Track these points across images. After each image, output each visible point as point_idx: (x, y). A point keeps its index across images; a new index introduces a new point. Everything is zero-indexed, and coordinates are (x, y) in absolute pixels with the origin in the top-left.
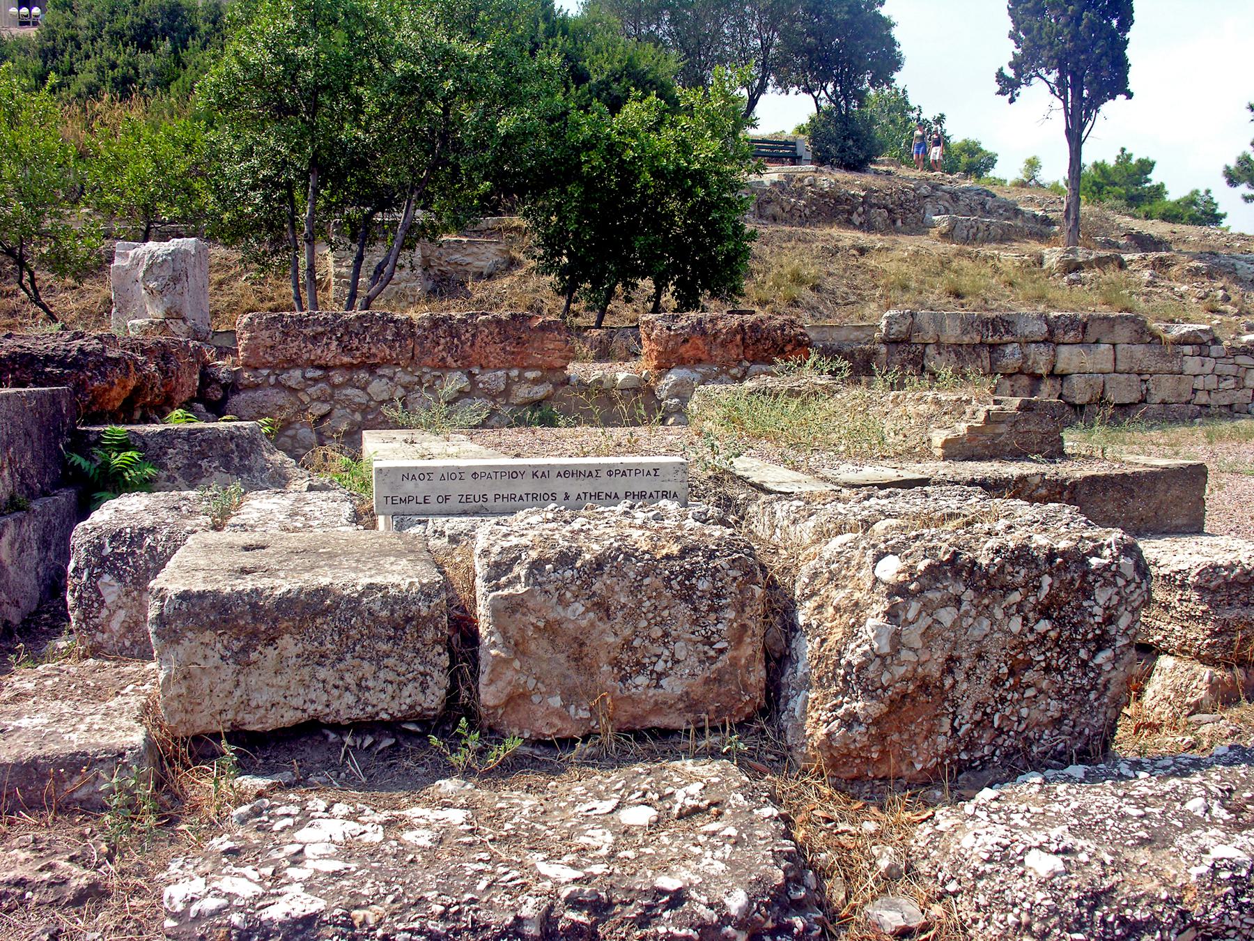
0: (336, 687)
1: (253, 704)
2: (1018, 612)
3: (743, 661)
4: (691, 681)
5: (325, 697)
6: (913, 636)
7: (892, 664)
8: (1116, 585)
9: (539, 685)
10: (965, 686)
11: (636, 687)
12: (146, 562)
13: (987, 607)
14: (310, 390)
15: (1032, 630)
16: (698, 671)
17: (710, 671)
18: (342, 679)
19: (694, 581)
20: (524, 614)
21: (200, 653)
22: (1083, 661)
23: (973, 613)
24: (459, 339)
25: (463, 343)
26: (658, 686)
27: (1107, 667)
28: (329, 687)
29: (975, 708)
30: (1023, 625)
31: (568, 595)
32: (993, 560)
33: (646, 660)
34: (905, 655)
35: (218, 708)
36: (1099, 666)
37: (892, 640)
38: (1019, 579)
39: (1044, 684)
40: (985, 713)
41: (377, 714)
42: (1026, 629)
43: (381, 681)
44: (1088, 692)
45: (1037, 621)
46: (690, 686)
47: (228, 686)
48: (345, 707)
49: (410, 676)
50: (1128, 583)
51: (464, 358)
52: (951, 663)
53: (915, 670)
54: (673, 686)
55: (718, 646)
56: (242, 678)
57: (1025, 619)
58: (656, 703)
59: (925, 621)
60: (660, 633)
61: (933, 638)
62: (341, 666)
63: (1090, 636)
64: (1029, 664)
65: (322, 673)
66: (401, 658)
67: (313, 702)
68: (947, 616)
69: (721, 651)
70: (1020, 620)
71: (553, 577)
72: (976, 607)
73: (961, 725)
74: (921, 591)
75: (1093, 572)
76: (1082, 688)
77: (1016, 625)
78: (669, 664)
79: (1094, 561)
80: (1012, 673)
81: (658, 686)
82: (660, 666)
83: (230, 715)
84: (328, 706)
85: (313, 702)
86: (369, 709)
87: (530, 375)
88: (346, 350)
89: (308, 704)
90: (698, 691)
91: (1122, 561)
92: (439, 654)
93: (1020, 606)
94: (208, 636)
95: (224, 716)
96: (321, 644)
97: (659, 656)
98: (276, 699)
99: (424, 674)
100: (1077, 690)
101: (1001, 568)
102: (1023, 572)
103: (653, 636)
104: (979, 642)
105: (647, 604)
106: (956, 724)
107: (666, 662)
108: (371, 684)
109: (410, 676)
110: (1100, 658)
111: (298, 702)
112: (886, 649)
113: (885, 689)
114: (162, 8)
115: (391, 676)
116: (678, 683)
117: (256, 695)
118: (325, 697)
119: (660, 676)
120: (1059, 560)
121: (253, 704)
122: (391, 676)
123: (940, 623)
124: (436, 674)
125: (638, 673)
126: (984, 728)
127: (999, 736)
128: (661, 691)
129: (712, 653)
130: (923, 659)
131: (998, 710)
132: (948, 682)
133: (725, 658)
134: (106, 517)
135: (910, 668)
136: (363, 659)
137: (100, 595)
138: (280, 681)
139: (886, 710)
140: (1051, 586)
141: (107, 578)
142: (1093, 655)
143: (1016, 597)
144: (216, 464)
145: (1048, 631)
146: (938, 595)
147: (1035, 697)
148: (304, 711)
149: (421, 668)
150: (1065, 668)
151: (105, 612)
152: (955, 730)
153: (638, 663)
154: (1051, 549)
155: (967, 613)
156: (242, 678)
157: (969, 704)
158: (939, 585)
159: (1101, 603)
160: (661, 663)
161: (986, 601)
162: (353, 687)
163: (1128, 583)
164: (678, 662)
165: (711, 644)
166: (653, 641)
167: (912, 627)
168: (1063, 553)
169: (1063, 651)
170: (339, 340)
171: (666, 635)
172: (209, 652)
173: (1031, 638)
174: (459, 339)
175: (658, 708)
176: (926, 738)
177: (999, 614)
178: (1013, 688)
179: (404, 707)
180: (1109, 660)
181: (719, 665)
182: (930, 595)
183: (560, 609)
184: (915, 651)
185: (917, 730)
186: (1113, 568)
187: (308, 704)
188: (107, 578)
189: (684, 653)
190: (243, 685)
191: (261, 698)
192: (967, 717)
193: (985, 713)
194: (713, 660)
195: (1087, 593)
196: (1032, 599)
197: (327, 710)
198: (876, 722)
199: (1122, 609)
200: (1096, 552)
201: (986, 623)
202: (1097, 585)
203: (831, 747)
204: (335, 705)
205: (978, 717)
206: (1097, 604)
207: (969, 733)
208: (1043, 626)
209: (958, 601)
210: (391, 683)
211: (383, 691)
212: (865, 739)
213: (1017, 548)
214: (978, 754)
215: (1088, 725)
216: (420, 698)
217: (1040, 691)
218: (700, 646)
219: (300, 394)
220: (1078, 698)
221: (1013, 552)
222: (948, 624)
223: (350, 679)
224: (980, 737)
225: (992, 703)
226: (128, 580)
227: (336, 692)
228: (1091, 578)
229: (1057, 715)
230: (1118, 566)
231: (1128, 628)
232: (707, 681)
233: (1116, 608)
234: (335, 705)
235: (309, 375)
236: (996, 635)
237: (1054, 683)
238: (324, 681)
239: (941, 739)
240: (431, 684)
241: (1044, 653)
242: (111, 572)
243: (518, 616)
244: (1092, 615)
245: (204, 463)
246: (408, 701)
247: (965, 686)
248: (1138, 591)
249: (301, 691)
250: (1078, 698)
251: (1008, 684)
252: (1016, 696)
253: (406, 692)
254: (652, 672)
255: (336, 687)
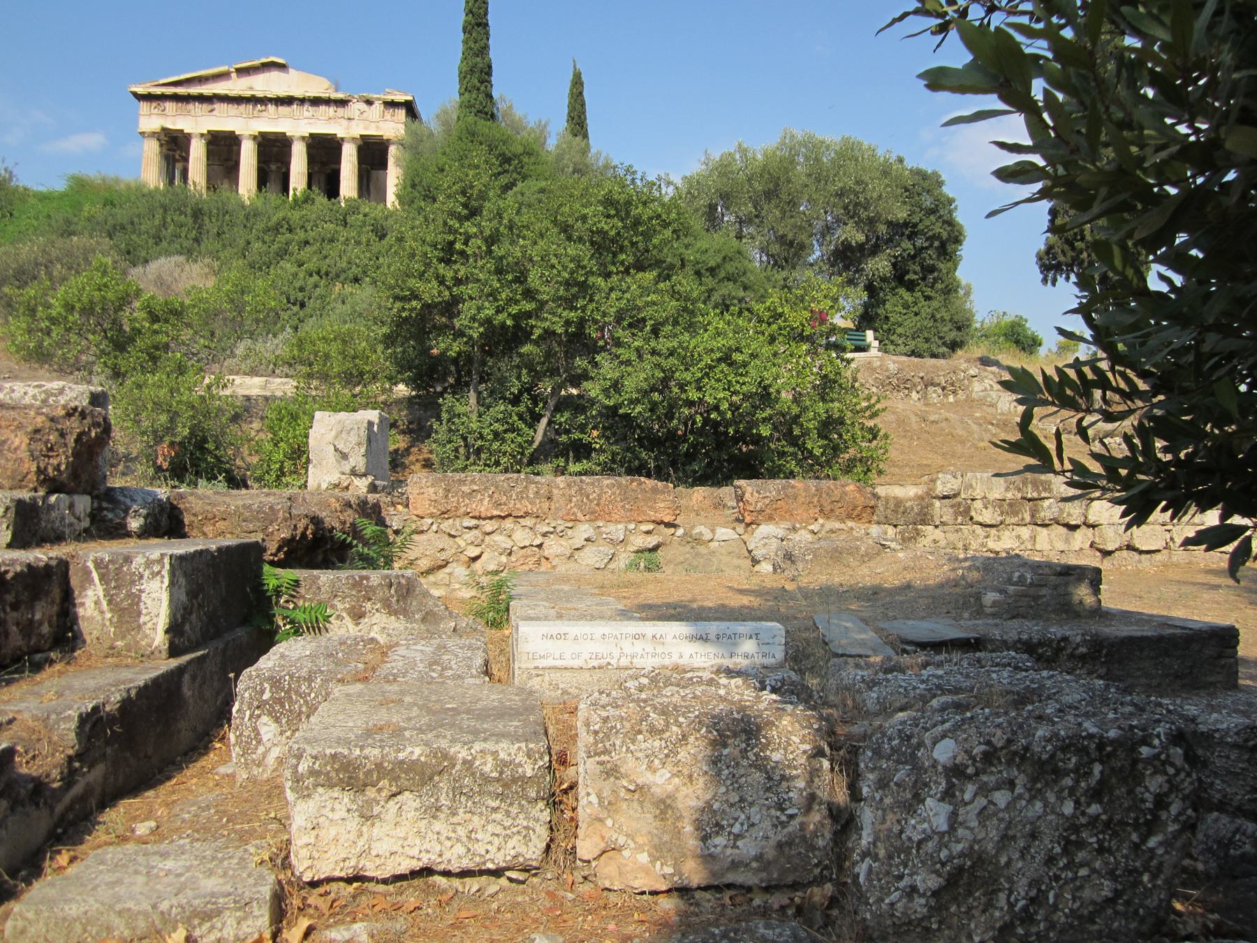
0: (449, 838)
1: (374, 853)
2: (1070, 795)
3: (812, 827)
4: (764, 843)
5: (438, 848)
6: (969, 815)
7: (950, 841)
8: (1166, 773)
9: (629, 841)
10: (1020, 864)
11: (715, 846)
12: (301, 706)
13: (1040, 790)
14: (466, 536)
15: (1083, 813)
16: (771, 834)
17: (781, 835)
18: (454, 831)
19: (768, 753)
20: (617, 778)
21: (329, 806)
22: (1135, 844)
23: (1027, 796)
24: (588, 497)
25: (591, 501)
26: (735, 846)
27: (1160, 851)
28: (442, 838)
29: (1030, 885)
30: (1075, 808)
31: (657, 762)
32: (1044, 747)
33: (725, 823)
34: (961, 832)
35: (343, 855)
36: (1152, 850)
37: (949, 818)
38: (1071, 766)
39: (1097, 864)
40: (1039, 890)
41: (484, 863)
42: (1078, 812)
43: (488, 835)
44: (1141, 874)
45: (1089, 805)
46: (763, 848)
47: (352, 836)
48: (456, 858)
49: (515, 830)
50: (1178, 771)
51: (592, 513)
52: (1006, 839)
53: (971, 847)
54: (748, 848)
55: (789, 812)
56: (365, 829)
57: (1077, 802)
58: (733, 861)
59: (982, 801)
60: (737, 799)
61: (989, 817)
62: (455, 820)
63: (1141, 821)
64: (1081, 844)
65: (437, 826)
66: (508, 813)
67: (428, 852)
68: (1001, 798)
69: (791, 817)
70: (1072, 804)
71: (643, 746)
72: (1029, 790)
73: (1017, 900)
74: (977, 774)
75: (1143, 761)
76: (1135, 870)
77: (1068, 808)
78: (745, 827)
79: (1145, 751)
80: (1065, 851)
81: (735, 846)
82: (736, 829)
83: (353, 863)
84: (440, 855)
85: (428, 852)
86: (477, 859)
87: (645, 527)
88: (498, 505)
89: (423, 854)
90: (770, 853)
91: (1172, 751)
92: (542, 811)
93: (1072, 791)
94: (336, 792)
95: (347, 863)
96: (437, 800)
97: (736, 819)
98: (394, 849)
99: (527, 828)
100: (1130, 872)
101: (1053, 756)
102: (1074, 760)
103: (732, 801)
104: (1031, 823)
105: (726, 772)
106: (1012, 899)
107: (742, 824)
108: (479, 836)
109: (515, 830)
110: (1152, 842)
111: (415, 852)
112: (944, 828)
113: (943, 864)
114: (511, 107)
115: (498, 830)
116: (753, 844)
117: (378, 844)
118: (438, 848)
119: (738, 837)
120: (1109, 749)
121: (374, 853)
122: (498, 830)
123: (995, 804)
124: (538, 829)
125: (717, 833)
126: (1040, 906)
127: (1054, 912)
128: (737, 851)
129: (784, 818)
130: (979, 837)
131: (1052, 888)
132: (1003, 860)
133: (795, 823)
134: (270, 664)
135: (967, 845)
136: (473, 813)
137: (258, 734)
138: (401, 832)
139: (944, 883)
140: (1102, 772)
141: (265, 719)
142: (1144, 839)
143: (1068, 781)
144: (379, 606)
145: (1099, 815)
146: (993, 778)
147: (1089, 876)
148: (419, 859)
149: (525, 823)
150: (1117, 850)
151: (261, 749)
152: (1011, 906)
153: (717, 824)
154: (1102, 737)
155: (1020, 797)
156: (365, 829)
157: (1024, 881)
158: (993, 769)
159: (1152, 789)
160: (737, 825)
161: (1039, 786)
162: (465, 839)
163: (1178, 771)
164: (753, 825)
165: (783, 810)
166: (732, 805)
167: (968, 808)
168: (1112, 742)
169: (1115, 834)
170: (491, 497)
171: (742, 800)
172: (337, 806)
173: (1083, 820)
174: (588, 497)
175: (735, 865)
176: (984, 911)
177: (1052, 798)
178: (1066, 867)
179: (509, 858)
180: (1161, 844)
181: (790, 829)
182: (985, 778)
183: (649, 774)
184: (971, 829)
185: (975, 904)
186: (1163, 757)
187: (423, 854)
188: (265, 719)
189: (758, 817)
190: (366, 836)
191: (381, 847)
192: (1023, 893)
193: (1039, 890)
194: (783, 825)
195: (1138, 779)
196: (1083, 784)
197: (440, 860)
198: (935, 894)
199: (1173, 796)
200: (1145, 741)
201: (1038, 805)
202: (1148, 772)
203: (893, 915)
204: (447, 855)
205: (1033, 893)
206: (1148, 791)
207: (1025, 909)
208: (1094, 809)
209: (1011, 784)
210: (497, 835)
211: (490, 843)
212: (925, 910)
213: (1068, 737)
214: (1034, 929)
215: (1141, 906)
216: (523, 849)
217: (1094, 871)
218: (773, 812)
219: (457, 539)
220: (1131, 879)
221: (1064, 740)
222: (1003, 806)
223: (462, 832)
224: (1036, 913)
225: (1046, 880)
226: (284, 721)
227: (449, 844)
228: (1140, 766)
229: (1110, 895)
230: (1168, 756)
231: (1180, 814)
232: (780, 846)
233: (1166, 795)
234: (447, 855)
235: (466, 524)
236: (1049, 817)
237: (1107, 864)
238: (438, 833)
239: (997, 914)
240: (533, 837)
241: (1096, 835)
242: (270, 714)
243: (612, 779)
244: (1143, 801)
245: (368, 605)
246: (513, 852)
247: (1020, 864)
248: (1188, 780)
249: (418, 841)
250: (1131, 879)
251: (1061, 864)
252: (1070, 875)
253: (511, 843)
254: (730, 833)
255: (449, 838)
